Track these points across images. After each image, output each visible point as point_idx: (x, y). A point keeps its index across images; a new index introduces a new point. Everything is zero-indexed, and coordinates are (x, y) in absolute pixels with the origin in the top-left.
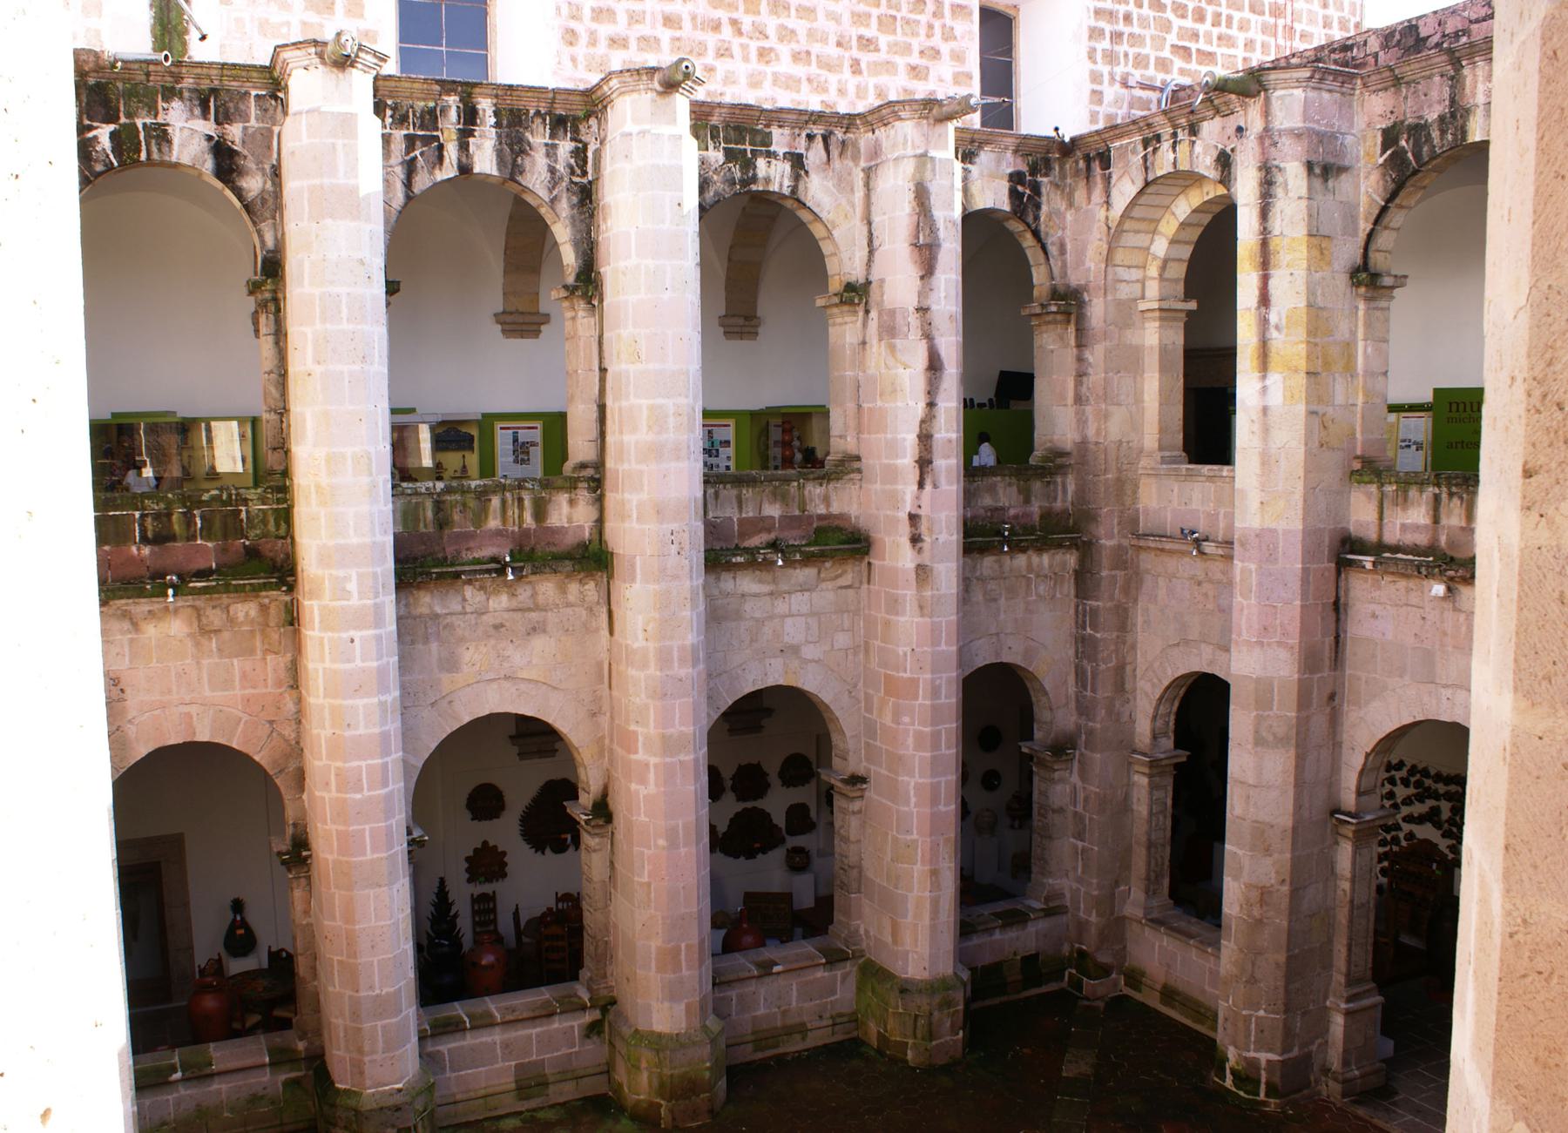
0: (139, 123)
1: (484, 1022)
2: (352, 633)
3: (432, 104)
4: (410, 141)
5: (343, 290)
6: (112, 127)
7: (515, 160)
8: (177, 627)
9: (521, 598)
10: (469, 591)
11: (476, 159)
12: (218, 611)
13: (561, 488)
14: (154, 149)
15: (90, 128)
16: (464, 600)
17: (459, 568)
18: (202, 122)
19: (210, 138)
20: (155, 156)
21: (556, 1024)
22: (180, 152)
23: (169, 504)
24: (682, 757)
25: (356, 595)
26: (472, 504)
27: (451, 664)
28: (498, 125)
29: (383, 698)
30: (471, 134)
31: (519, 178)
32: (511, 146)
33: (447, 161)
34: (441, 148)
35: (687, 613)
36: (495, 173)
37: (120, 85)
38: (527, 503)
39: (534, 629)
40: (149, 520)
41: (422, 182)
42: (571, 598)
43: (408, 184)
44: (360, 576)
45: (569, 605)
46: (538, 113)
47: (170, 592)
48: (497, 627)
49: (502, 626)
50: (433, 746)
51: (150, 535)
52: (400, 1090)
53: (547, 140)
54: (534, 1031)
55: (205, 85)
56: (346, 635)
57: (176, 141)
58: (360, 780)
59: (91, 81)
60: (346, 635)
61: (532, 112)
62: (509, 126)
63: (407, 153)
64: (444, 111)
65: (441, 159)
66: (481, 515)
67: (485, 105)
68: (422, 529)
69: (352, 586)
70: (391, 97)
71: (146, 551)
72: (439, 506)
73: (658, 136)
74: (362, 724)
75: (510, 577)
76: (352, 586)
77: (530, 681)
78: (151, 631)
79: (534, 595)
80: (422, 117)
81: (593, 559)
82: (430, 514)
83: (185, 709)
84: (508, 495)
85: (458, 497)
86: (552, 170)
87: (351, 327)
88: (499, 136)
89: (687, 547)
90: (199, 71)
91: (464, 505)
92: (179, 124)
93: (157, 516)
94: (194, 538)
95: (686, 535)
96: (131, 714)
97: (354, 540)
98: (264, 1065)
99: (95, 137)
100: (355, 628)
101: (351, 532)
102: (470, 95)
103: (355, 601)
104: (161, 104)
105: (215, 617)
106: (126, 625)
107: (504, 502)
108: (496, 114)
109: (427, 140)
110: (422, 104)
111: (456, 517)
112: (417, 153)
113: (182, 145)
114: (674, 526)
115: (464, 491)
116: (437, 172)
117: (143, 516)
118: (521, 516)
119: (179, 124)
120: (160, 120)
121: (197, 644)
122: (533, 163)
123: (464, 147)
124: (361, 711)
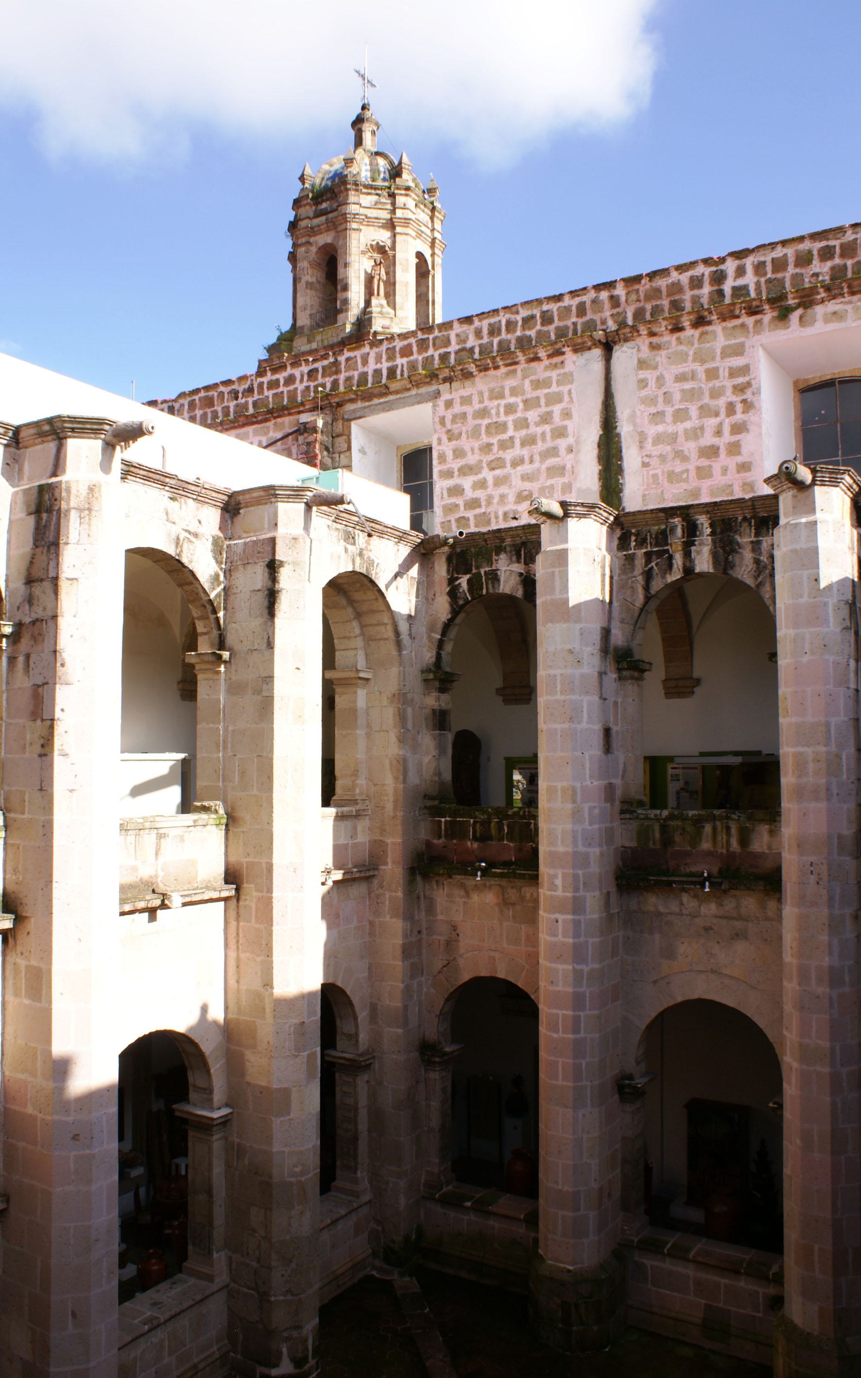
0: (482, 571)
1: (679, 1254)
2: (557, 916)
3: (663, 527)
4: (648, 556)
5: (558, 672)
6: (468, 576)
7: (727, 559)
8: (490, 898)
9: (727, 908)
10: (685, 898)
11: (697, 562)
12: (515, 891)
13: (762, 821)
14: (490, 586)
15: (457, 579)
16: (682, 904)
17: (671, 879)
18: (516, 565)
19: (521, 574)
20: (491, 591)
21: (742, 1283)
22: (504, 586)
23: (489, 815)
24: (818, 1068)
25: (560, 888)
26: (689, 829)
27: (669, 953)
28: (712, 534)
29: (579, 967)
30: (692, 543)
31: (731, 572)
32: (723, 548)
33: (675, 566)
34: (671, 557)
35: (824, 938)
36: (711, 571)
37: (473, 549)
38: (734, 831)
39: (737, 935)
40: (478, 825)
41: (657, 585)
42: (770, 914)
43: (647, 588)
44: (564, 875)
45: (767, 919)
46: (745, 519)
47: (479, 873)
48: (707, 929)
49: (711, 928)
50: (653, 1015)
51: (478, 835)
52: (569, 1271)
53: (753, 539)
54: (724, 1281)
55: (518, 541)
56: (553, 916)
57: (502, 579)
58: (558, 1024)
59: (458, 550)
60: (553, 916)
61: (740, 518)
62: (722, 532)
63: (646, 565)
64: (673, 529)
65: (670, 566)
66: (697, 836)
67: (703, 521)
68: (651, 845)
69: (559, 882)
70: (634, 527)
71: (476, 845)
72: (664, 829)
73: (796, 525)
74: (561, 983)
75: (707, 890)
76: (559, 882)
77: (731, 977)
78: (475, 898)
79: (738, 907)
80: (657, 537)
81: (770, 882)
82: (657, 835)
83: (492, 954)
84: (718, 823)
85: (679, 823)
86: (757, 562)
87: (563, 697)
88: (714, 541)
89: (825, 878)
90: (511, 533)
91: (684, 829)
92: (504, 569)
93: (483, 823)
94: (503, 839)
95: (825, 868)
96: (462, 951)
97: (561, 849)
98: (520, 1220)
99: (460, 584)
100: (560, 912)
101: (559, 843)
102: (688, 515)
103: (559, 893)
104: (495, 557)
105: (512, 894)
106: (462, 893)
107: (714, 829)
108: (711, 525)
109: (660, 554)
110: (656, 528)
111: (677, 838)
112: (653, 564)
113: (505, 582)
114: (812, 858)
115: (684, 819)
116: (668, 576)
117: (475, 822)
118: (728, 842)
119: (504, 569)
120: (494, 568)
121: (501, 911)
122: (742, 558)
123: (687, 554)
124: (560, 973)
